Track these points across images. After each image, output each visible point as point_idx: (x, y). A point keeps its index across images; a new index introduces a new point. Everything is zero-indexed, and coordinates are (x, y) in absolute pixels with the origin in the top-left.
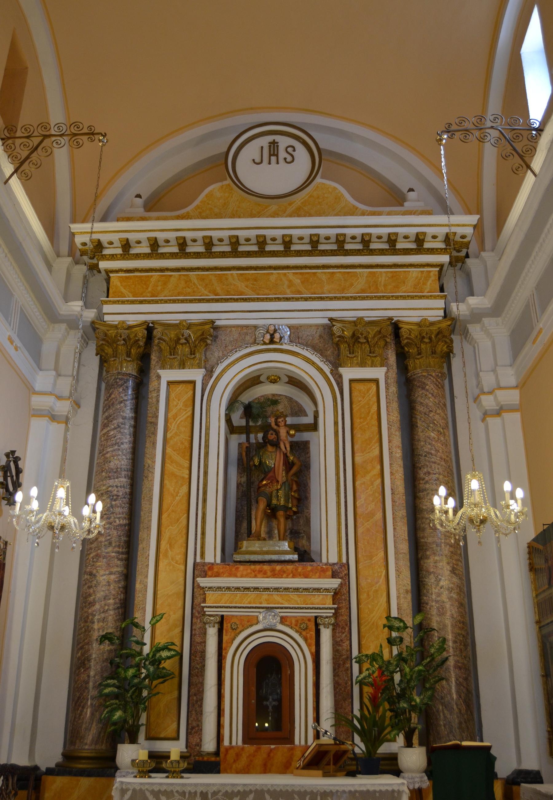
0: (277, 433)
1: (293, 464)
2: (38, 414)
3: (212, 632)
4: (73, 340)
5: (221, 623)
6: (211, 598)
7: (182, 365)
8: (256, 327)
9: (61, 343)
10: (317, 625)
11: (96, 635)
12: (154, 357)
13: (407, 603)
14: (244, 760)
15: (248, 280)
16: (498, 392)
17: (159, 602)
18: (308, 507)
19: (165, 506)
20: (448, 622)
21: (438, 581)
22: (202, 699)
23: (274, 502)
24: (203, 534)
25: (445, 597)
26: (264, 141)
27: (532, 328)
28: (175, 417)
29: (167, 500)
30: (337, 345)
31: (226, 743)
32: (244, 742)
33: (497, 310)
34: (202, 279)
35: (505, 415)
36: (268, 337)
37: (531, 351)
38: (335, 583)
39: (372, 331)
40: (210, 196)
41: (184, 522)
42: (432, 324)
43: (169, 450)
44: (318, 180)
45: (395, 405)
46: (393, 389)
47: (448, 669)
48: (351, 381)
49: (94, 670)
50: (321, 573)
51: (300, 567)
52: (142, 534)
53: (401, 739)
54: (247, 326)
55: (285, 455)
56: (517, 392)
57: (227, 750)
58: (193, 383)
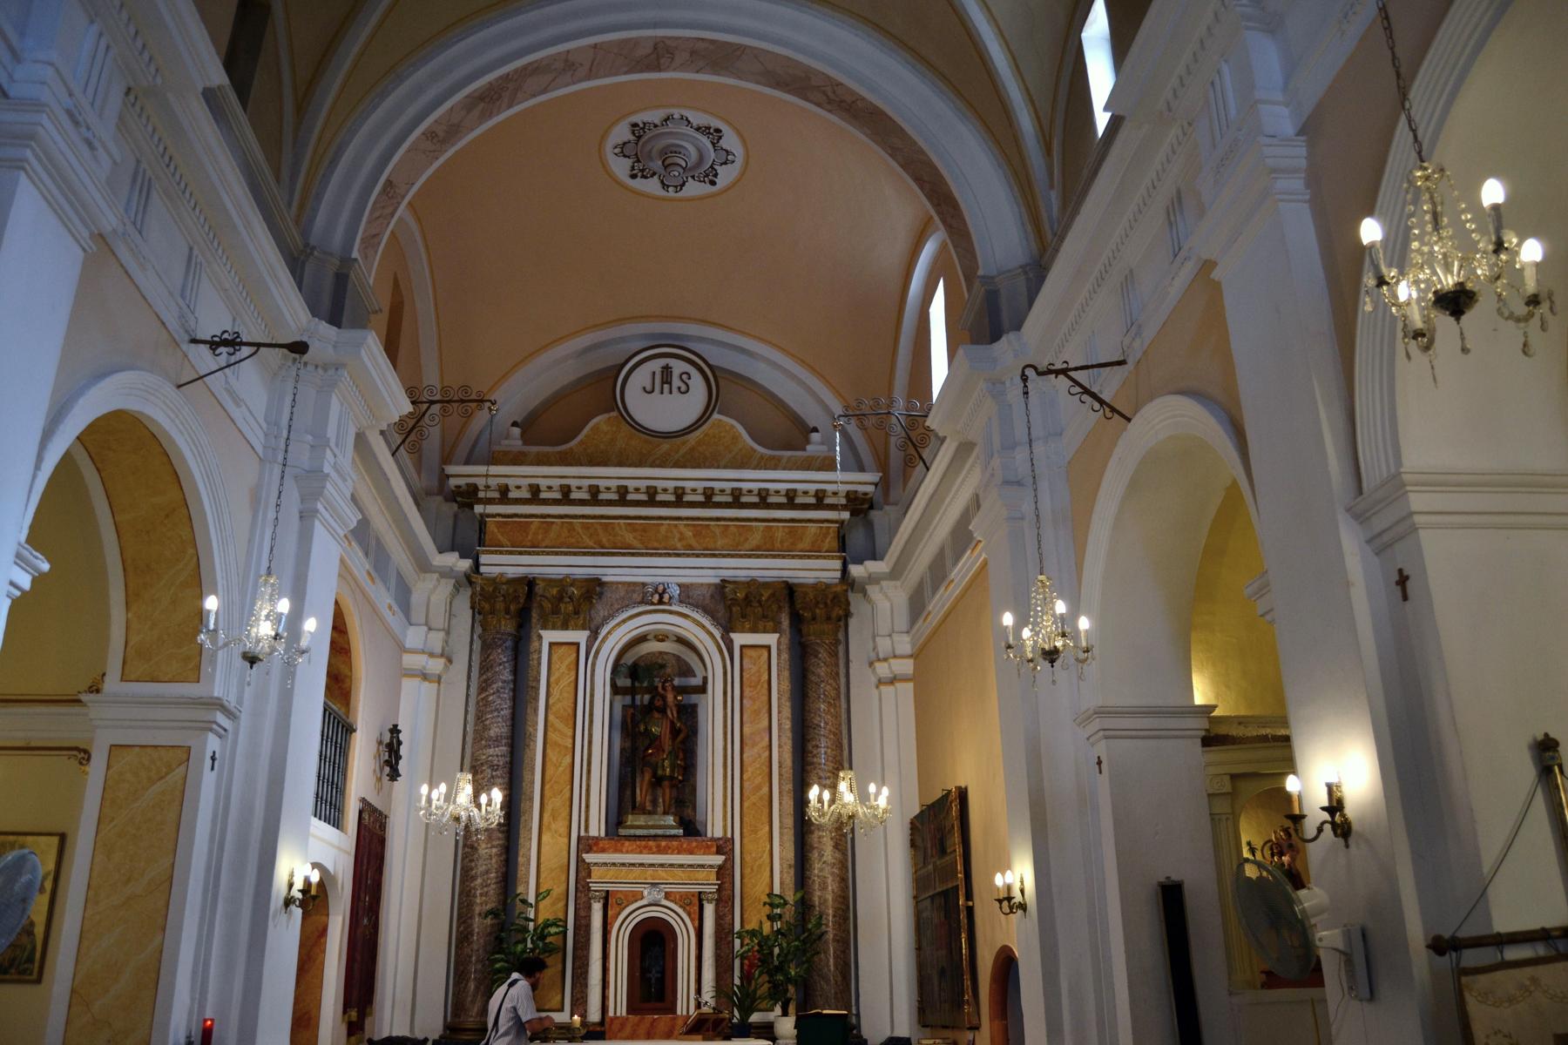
0: (664, 698)
1: (679, 731)
2: (411, 674)
3: (597, 908)
4: (447, 587)
6: (596, 874)
8: (644, 585)
9: (433, 594)
10: (701, 901)
11: (477, 909)
12: (535, 615)
13: (790, 879)
14: (628, 1029)
15: (635, 530)
17: (543, 876)
18: (694, 775)
19: (547, 778)
20: (830, 897)
22: (587, 972)
23: (660, 772)
24: (587, 806)
25: (826, 873)
26: (656, 365)
31: (611, 1014)
32: (628, 1012)
33: (895, 574)
34: (586, 527)
35: (898, 685)
36: (656, 597)
37: (925, 627)
39: (766, 594)
40: (596, 428)
41: (568, 795)
42: (828, 586)
43: (551, 717)
44: (716, 416)
45: (786, 674)
46: (785, 656)
47: (826, 942)
48: (742, 647)
49: (478, 941)
50: (706, 850)
51: (685, 842)
52: (524, 806)
53: (778, 1010)
54: (635, 584)
55: (672, 723)
57: (612, 1019)
58: (578, 645)
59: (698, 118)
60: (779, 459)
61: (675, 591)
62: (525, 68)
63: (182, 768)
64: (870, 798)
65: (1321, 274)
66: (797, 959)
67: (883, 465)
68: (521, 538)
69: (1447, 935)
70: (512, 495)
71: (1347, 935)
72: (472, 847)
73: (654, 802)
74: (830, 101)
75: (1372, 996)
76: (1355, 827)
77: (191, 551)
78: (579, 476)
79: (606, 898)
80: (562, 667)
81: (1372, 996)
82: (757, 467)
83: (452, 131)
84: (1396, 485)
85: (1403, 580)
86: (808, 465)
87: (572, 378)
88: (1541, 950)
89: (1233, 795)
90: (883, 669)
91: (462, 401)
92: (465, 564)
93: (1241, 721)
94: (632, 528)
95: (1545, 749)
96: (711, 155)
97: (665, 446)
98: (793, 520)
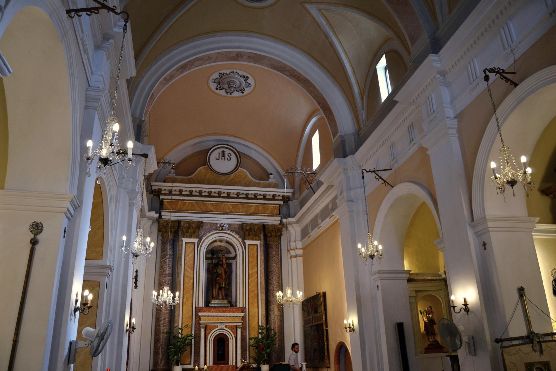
0: (222, 261)
3: (203, 330)
4: (150, 222)
5: (206, 327)
7: (190, 237)
8: (216, 224)
10: (236, 328)
12: (180, 233)
13: (264, 321)
16: (296, 250)
21: (274, 313)
26: (220, 151)
27: (308, 234)
28: (188, 255)
29: (186, 285)
30: (244, 232)
33: (297, 222)
34: (197, 204)
35: (298, 258)
36: (221, 228)
37: (307, 240)
38: (242, 314)
42: (276, 225)
43: (186, 267)
44: (240, 168)
45: (263, 254)
46: (262, 248)
56: (302, 250)
58: (194, 243)
59: (241, 73)
60: (260, 183)
61: (226, 226)
62: (196, 58)
63: (98, 288)
64: (292, 295)
65: (461, 159)
66: (268, 345)
67: (292, 185)
68: (175, 207)
69: (499, 338)
70: (173, 193)
71: (469, 338)
72: (160, 310)
73: (218, 295)
74: (291, 75)
75: (475, 354)
76: (470, 309)
77: (102, 218)
78: (196, 187)
79: (206, 327)
80: (189, 250)
81: (475, 354)
82: (253, 186)
83: (172, 77)
84: (484, 219)
85: (484, 244)
86: (269, 186)
87: (190, 153)
88: (520, 342)
89: (416, 297)
90: (293, 253)
91: (163, 163)
92: (157, 215)
93: (417, 274)
94: (213, 205)
95: (521, 291)
96: (244, 84)
97: (223, 178)
98: (265, 204)
